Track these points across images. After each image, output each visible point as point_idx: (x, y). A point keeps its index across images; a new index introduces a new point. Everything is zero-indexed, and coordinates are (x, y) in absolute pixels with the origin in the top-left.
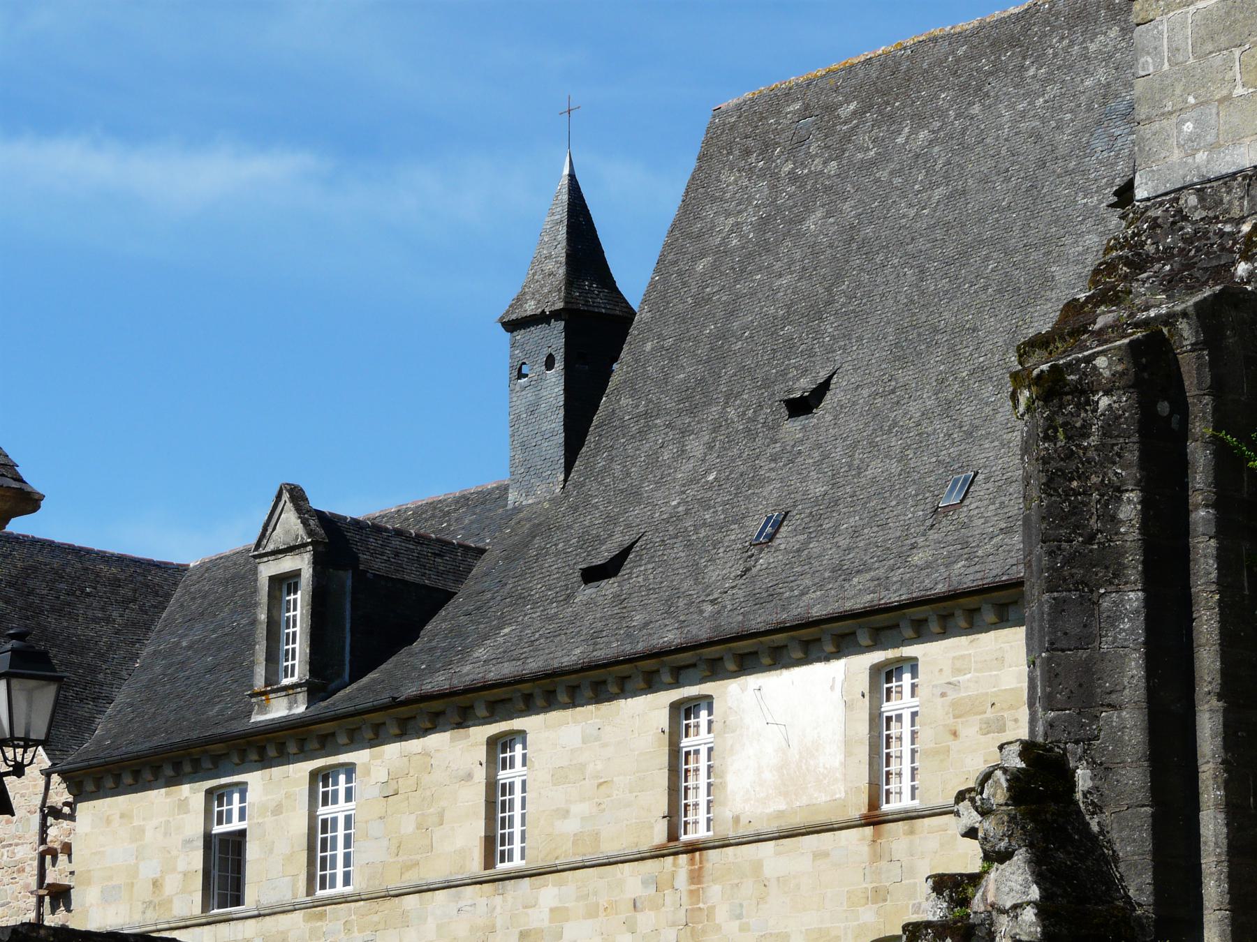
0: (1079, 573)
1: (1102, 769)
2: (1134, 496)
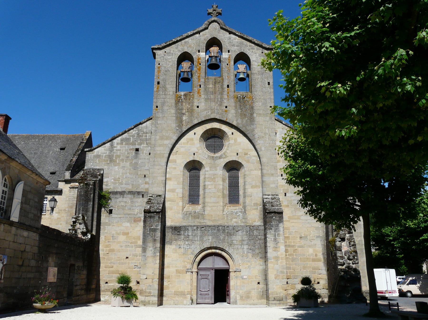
0: (87, 200)
1: (87, 217)
2: (92, 195)
